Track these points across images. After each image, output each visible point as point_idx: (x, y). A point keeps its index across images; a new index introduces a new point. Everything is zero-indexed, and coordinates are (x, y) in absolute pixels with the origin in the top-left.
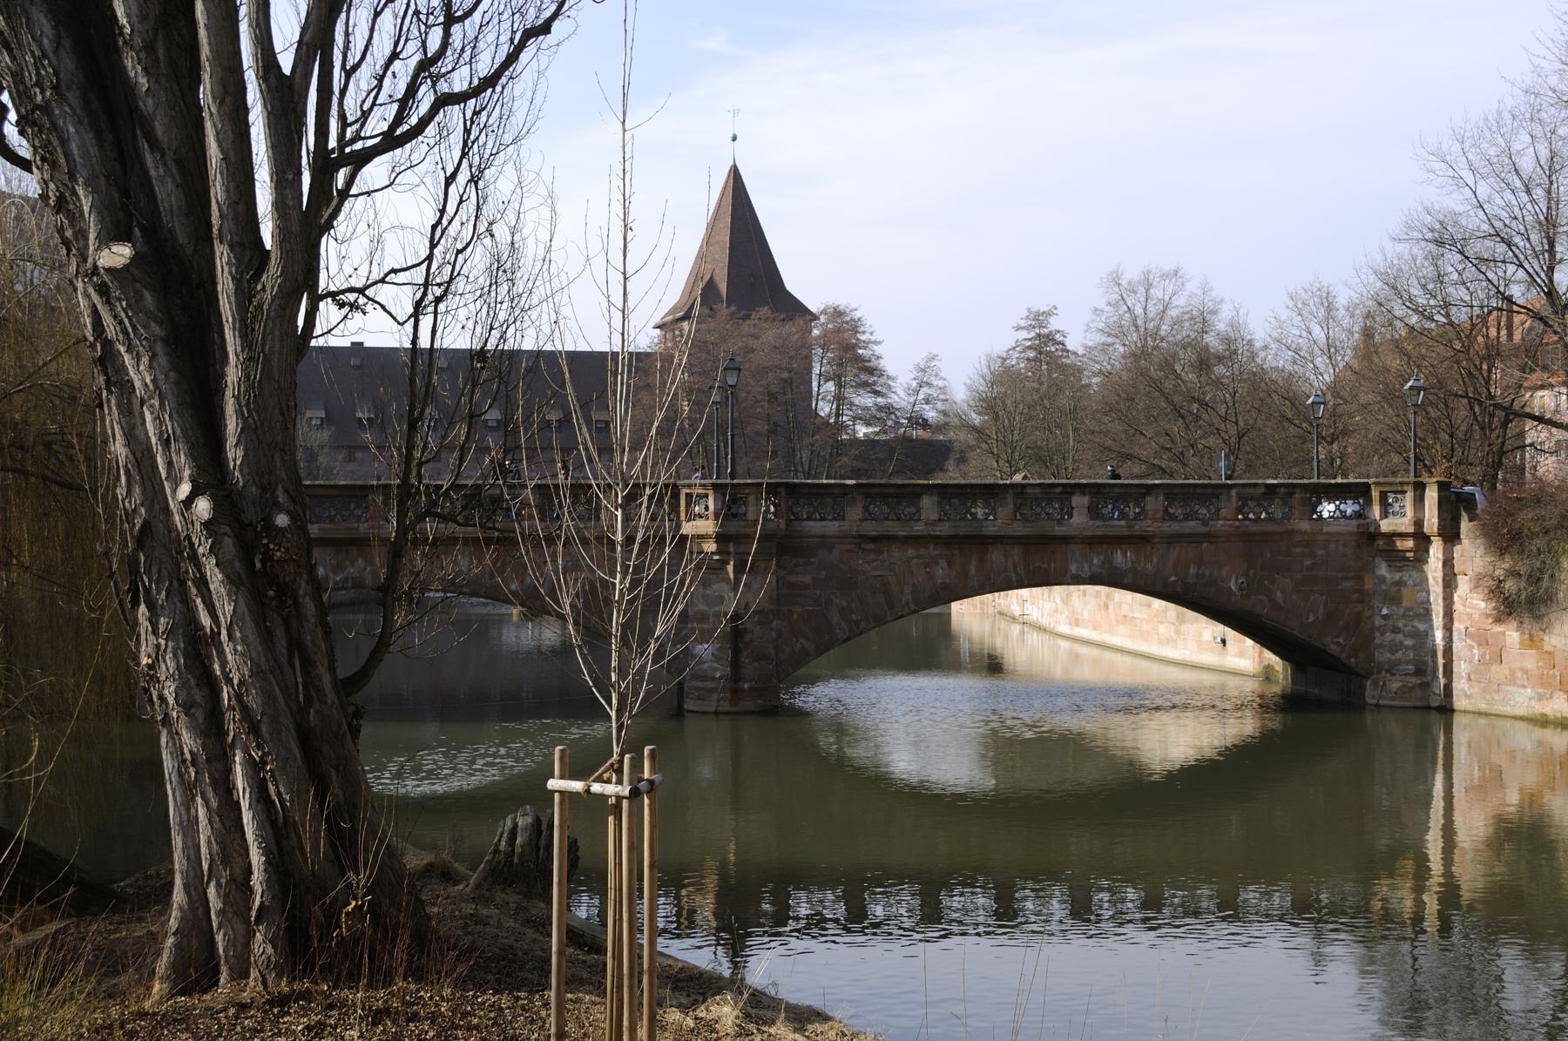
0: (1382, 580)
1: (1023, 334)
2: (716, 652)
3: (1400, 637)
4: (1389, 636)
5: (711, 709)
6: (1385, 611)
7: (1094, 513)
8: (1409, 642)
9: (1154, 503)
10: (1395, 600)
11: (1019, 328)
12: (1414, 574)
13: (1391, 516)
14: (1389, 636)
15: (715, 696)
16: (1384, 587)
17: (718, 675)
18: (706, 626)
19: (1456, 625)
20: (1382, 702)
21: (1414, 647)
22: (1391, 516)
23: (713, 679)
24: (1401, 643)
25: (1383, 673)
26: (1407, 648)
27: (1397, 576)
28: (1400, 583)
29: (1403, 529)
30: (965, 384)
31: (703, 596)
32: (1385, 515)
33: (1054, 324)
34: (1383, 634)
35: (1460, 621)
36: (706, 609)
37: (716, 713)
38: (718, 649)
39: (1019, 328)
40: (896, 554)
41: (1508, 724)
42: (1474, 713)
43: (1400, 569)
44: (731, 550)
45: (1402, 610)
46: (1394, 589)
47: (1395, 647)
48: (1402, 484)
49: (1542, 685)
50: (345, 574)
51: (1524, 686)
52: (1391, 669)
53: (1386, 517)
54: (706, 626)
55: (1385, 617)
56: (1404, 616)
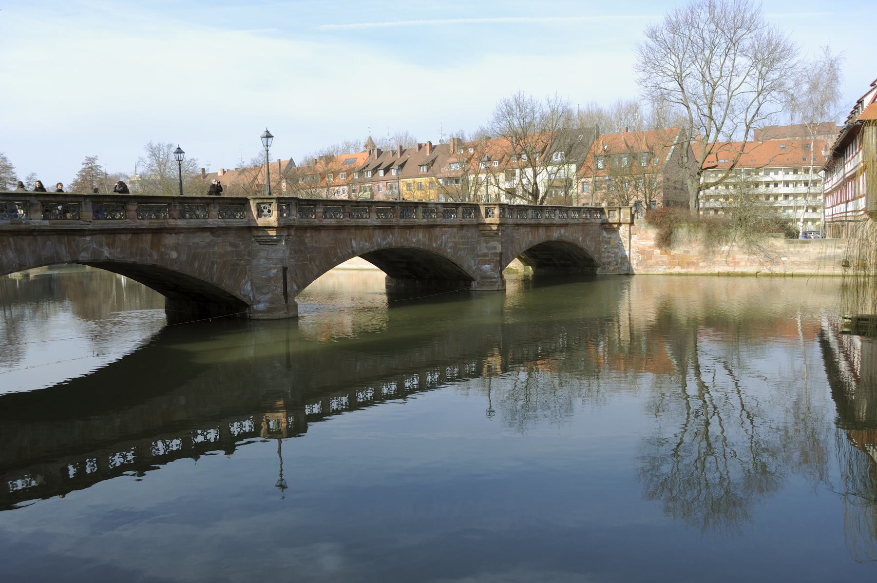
0: (605, 237)
1: (84, 166)
2: (492, 268)
3: (610, 254)
4: (606, 254)
5: (496, 289)
6: (605, 247)
7: (97, 214)
8: (613, 255)
9: (320, 210)
10: (608, 243)
11: (83, 164)
12: (614, 235)
13: (263, 217)
14: (606, 254)
15: (497, 284)
16: (605, 239)
17: (496, 276)
18: (487, 258)
19: (632, 249)
20: (607, 274)
21: (614, 257)
22: (263, 217)
23: (495, 278)
24: (610, 256)
25: (606, 265)
26: (612, 257)
27: (609, 236)
28: (610, 238)
29: (615, 222)
30: (14, 168)
31: (486, 247)
32: (259, 216)
33: (97, 163)
34: (605, 253)
35: (633, 248)
36: (488, 252)
37: (498, 290)
38: (493, 267)
39: (83, 164)
40: (323, 234)
41: (655, 276)
42: (639, 274)
43: (610, 234)
44: (500, 229)
45: (611, 246)
46: (608, 240)
47: (608, 257)
48: (615, 208)
49: (670, 265)
50: (386, 241)
51: (662, 265)
52: (609, 264)
53: (261, 217)
54: (487, 258)
55: (606, 248)
56: (611, 248)
